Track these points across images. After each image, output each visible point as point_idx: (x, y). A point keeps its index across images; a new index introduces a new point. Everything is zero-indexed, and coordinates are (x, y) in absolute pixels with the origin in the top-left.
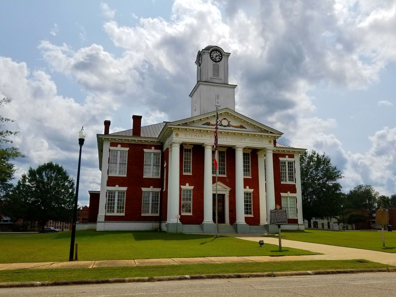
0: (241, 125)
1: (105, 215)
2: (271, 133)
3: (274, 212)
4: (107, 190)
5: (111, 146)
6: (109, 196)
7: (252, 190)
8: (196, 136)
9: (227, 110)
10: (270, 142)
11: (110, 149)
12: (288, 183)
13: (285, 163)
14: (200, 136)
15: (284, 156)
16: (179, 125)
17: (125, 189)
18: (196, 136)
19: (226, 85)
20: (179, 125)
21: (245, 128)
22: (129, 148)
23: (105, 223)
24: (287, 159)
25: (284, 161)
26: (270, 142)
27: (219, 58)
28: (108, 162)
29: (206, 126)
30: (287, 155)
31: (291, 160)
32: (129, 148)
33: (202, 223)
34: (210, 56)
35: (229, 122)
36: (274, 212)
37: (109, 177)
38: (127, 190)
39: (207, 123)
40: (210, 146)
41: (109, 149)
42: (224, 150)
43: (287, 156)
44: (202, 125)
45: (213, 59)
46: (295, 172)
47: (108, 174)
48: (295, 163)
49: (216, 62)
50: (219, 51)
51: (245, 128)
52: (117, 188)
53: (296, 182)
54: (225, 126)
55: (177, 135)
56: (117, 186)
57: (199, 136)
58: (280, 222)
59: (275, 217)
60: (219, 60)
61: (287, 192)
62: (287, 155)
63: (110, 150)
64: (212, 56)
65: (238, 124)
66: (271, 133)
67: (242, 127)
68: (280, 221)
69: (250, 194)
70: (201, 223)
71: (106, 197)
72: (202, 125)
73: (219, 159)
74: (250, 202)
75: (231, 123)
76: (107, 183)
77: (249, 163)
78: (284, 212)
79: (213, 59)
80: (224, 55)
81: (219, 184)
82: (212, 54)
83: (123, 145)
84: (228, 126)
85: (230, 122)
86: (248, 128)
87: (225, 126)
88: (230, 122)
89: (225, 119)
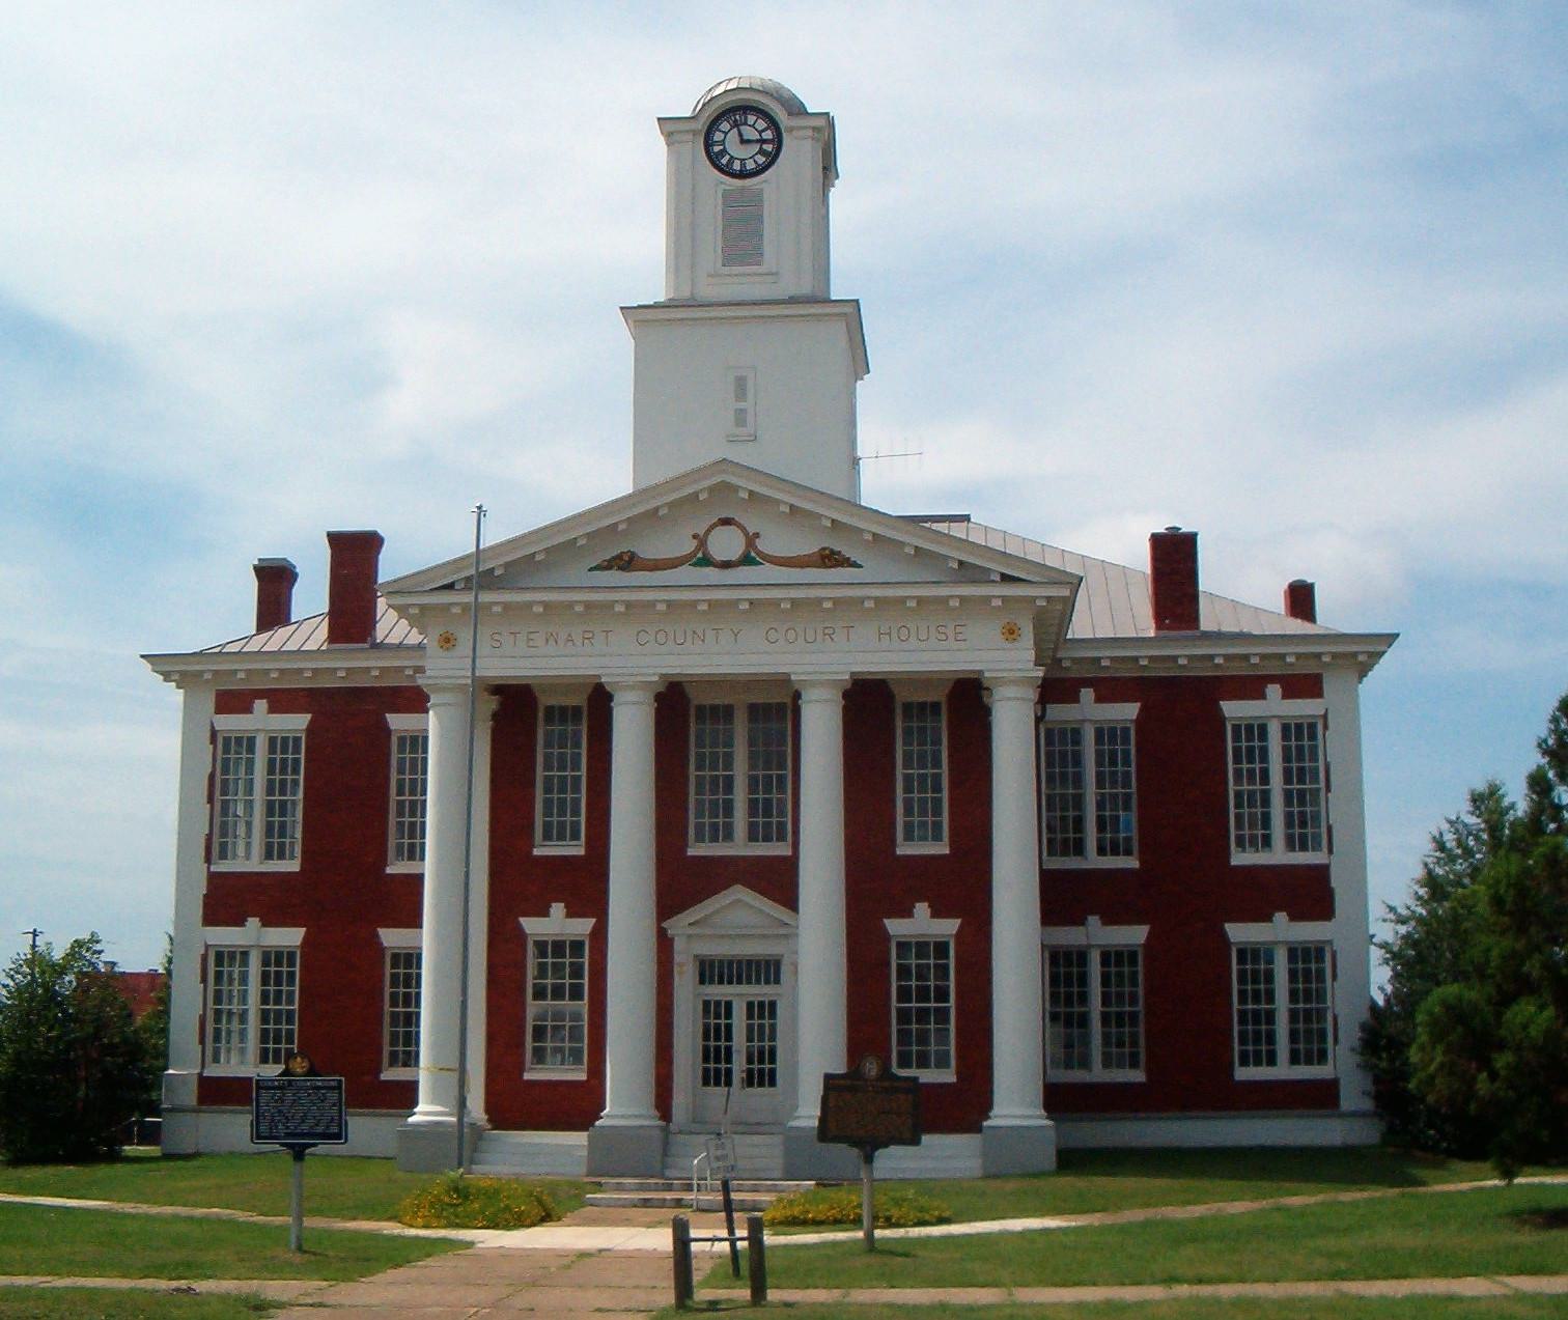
0: (824, 549)
1: (200, 1075)
2: (1006, 578)
3: (274, 1088)
4: (207, 947)
5: (219, 710)
6: (219, 976)
7: (948, 927)
8: (552, 642)
9: (724, 471)
10: (1011, 632)
11: (217, 728)
12: (1279, 855)
13: (1263, 730)
14: (539, 640)
15: (1252, 687)
16: (450, 587)
17: (290, 937)
18: (552, 642)
19: (828, 309)
20: (450, 587)
21: (855, 565)
22: (309, 716)
23: (201, 1114)
24: (1274, 706)
25: (1305, 721)
26: (1011, 632)
27: (761, 152)
28: (205, 800)
29: (615, 577)
30: (1273, 679)
31: (1303, 708)
32: (309, 716)
33: (597, 1123)
34: (708, 145)
35: (751, 540)
36: (274, 1088)
37: (213, 878)
38: (302, 944)
39: (619, 557)
40: (633, 688)
41: (212, 724)
42: (939, 696)
43: (1274, 691)
44: (591, 570)
45: (724, 161)
46: (1328, 789)
47: (208, 860)
48: (1326, 727)
49: (743, 174)
50: (746, 109)
51: (855, 565)
52: (251, 934)
53: (1330, 851)
54: (726, 565)
55: (447, 640)
56: (253, 922)
57: (570, 639)
58: (303, 1135)
59: (280, 1111)
60: (761, 159)
61: (1268, 918)
62: (1273, 679)
63: (214, 734)
64: (717, 149)
65: (809, 546)
66: (1006, 578)
67: (830, 559)
68: (305, 1128)
69: (941, 949)
70: (593, 1125)
71: (204, 980)
72: (591, 570)
73: (751, 752)
74: (942, 995)
75: (761, 544)
76: (206, 906)
77: (937, 764)
78: (333, 1088)
79: (724, 161)
80: (791, 130)
81: (739, 896)
82: (718, 136)
83: (281, 701)
84: (746, 560)
85: (757, 535)
86: (873, 568)
87: (726, 565)
88: (757, 535)
89: (726, 522)
